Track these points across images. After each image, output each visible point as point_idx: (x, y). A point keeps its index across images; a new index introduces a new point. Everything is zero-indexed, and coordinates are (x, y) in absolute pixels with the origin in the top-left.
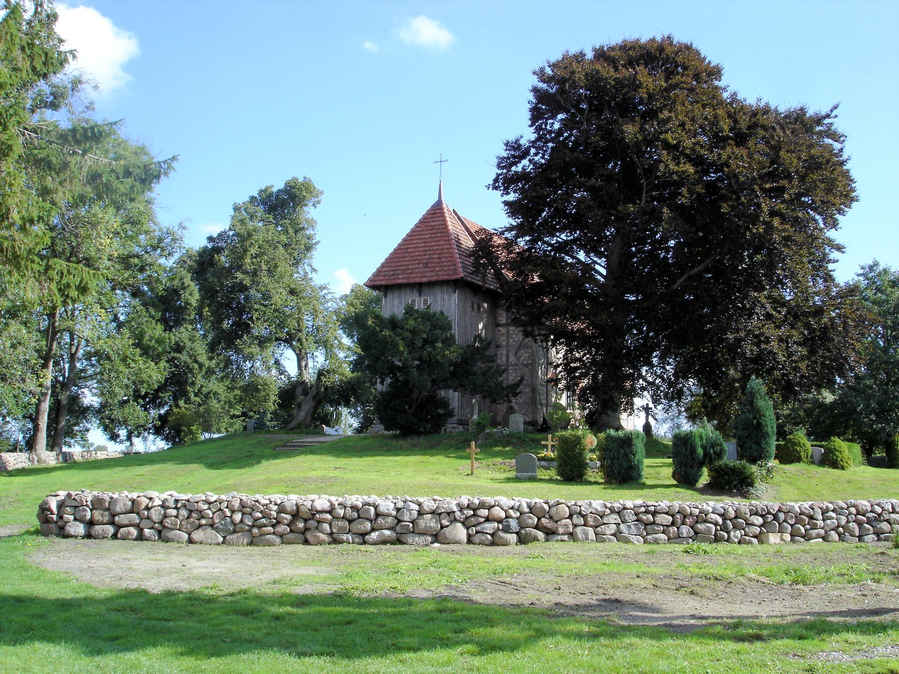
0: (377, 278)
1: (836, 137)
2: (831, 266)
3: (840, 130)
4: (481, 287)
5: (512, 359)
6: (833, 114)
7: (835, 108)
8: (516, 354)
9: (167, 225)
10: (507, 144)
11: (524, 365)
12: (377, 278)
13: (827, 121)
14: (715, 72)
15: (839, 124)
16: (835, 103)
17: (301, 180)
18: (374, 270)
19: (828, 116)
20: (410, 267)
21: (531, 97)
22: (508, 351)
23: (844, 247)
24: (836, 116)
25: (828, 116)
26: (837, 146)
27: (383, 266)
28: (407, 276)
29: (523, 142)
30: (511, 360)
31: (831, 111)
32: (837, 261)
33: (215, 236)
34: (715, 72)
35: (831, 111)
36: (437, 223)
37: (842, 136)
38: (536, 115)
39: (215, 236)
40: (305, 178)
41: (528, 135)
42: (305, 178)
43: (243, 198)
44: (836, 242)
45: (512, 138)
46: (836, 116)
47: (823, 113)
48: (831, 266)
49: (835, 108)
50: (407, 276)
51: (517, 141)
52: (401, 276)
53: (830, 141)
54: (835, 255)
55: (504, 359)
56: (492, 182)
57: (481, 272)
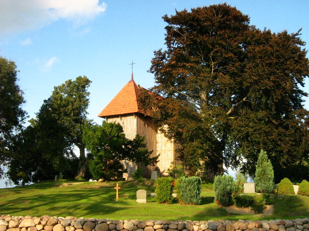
0: (103, 113)
1: (302, 43)
2: (302, 103)
3: (302, 41)
4: (144, 115)
5: (163, 148)
6: (299, 34)
7: (300, 30)
8: (165, 146)
9: (169, 143)
10: (155, 52)
11: (168, 150)
12: (103, 113)
13: (297, 37)
14: (246, 18)
15: (302, 38)
16: (301, 28)
17: (83, 77)
18: (102, 110)
19: (297, 34)
20: (117, 108)
21: (165, 32)
22: (162, 144)
23: (307, 94)
24: (301, 34)
25: (297, 34)
26: (302, 48)
27: (106, 108)
28: (115, 111)
29: (162, 51)
30: (163, 148)
31: (299, 32)
32: (305, 101)
33: (47, 99)
34: (269, 33)
35: (299, 32)
36: (130, 89)
37: (304, 42)
38: (168, 41)
39: (47, 99)
40: (84, 76)
41: (165, 48)
42: (84, 76)
43: (59, 84)
44: (304, 92)
45: (157, 50)
46: (301, 34)
47: (295, 33)
48: (302, 103)
49: (300, 30)
50: (115, 111)
51: (160, 51)
52: (113, 112)
53: (299, 46)
54: (303, 98)
55: (160, 148)
56: (149, 69)
57: (75, 81)
